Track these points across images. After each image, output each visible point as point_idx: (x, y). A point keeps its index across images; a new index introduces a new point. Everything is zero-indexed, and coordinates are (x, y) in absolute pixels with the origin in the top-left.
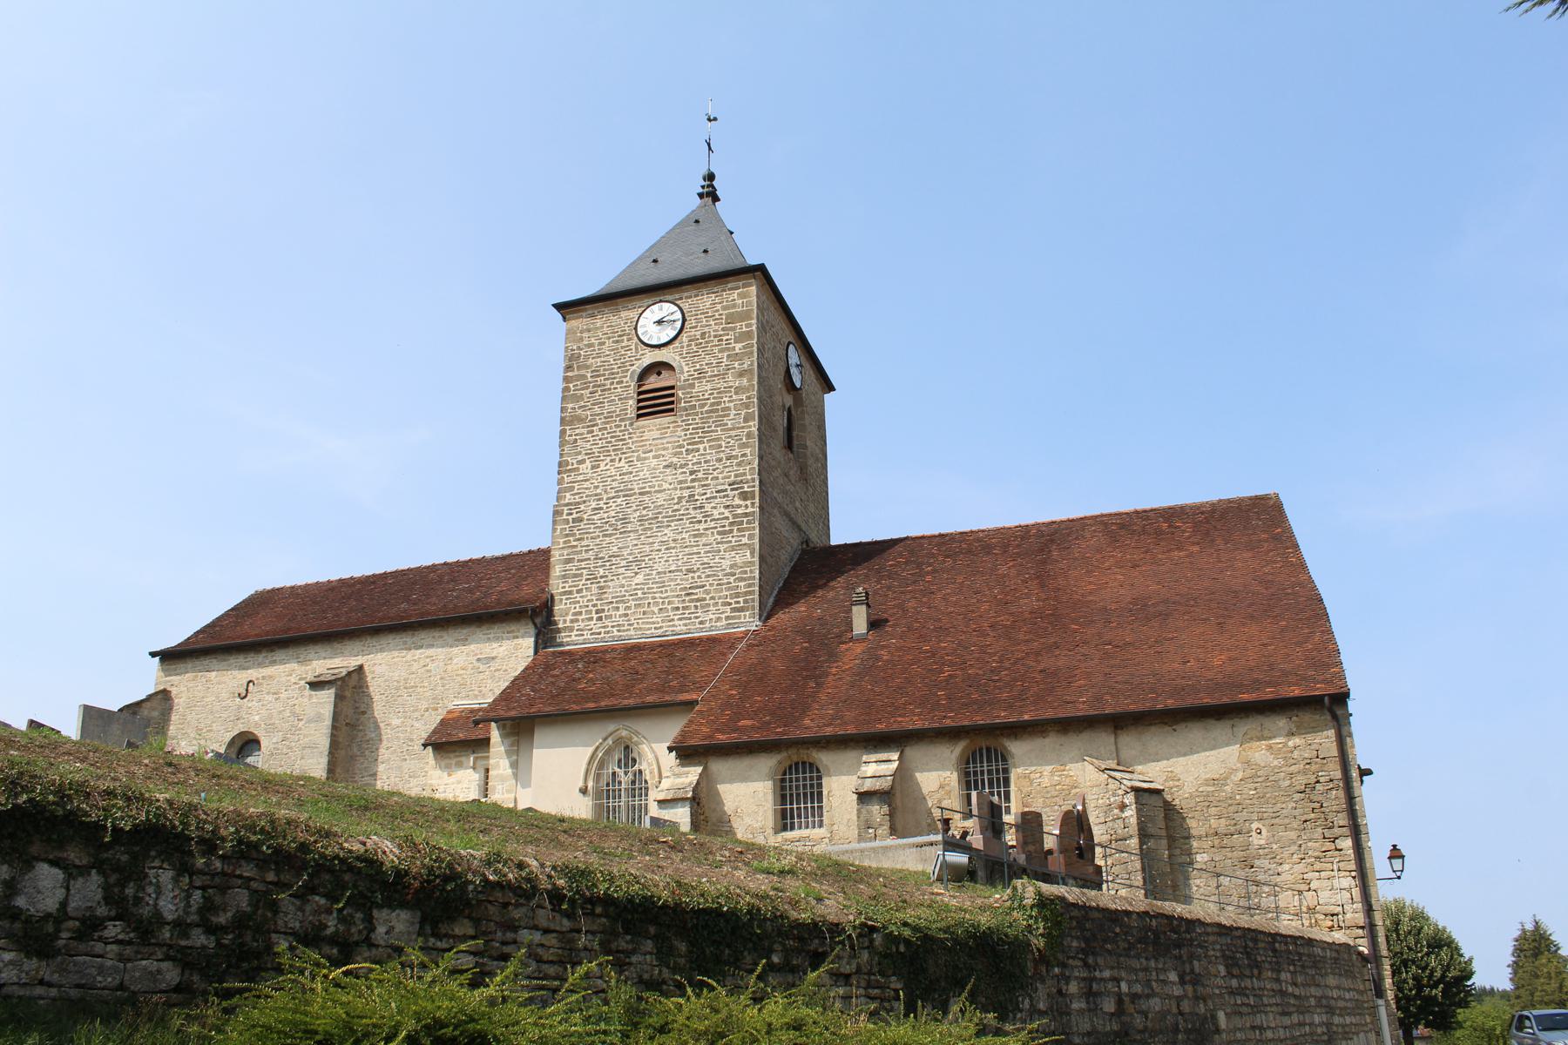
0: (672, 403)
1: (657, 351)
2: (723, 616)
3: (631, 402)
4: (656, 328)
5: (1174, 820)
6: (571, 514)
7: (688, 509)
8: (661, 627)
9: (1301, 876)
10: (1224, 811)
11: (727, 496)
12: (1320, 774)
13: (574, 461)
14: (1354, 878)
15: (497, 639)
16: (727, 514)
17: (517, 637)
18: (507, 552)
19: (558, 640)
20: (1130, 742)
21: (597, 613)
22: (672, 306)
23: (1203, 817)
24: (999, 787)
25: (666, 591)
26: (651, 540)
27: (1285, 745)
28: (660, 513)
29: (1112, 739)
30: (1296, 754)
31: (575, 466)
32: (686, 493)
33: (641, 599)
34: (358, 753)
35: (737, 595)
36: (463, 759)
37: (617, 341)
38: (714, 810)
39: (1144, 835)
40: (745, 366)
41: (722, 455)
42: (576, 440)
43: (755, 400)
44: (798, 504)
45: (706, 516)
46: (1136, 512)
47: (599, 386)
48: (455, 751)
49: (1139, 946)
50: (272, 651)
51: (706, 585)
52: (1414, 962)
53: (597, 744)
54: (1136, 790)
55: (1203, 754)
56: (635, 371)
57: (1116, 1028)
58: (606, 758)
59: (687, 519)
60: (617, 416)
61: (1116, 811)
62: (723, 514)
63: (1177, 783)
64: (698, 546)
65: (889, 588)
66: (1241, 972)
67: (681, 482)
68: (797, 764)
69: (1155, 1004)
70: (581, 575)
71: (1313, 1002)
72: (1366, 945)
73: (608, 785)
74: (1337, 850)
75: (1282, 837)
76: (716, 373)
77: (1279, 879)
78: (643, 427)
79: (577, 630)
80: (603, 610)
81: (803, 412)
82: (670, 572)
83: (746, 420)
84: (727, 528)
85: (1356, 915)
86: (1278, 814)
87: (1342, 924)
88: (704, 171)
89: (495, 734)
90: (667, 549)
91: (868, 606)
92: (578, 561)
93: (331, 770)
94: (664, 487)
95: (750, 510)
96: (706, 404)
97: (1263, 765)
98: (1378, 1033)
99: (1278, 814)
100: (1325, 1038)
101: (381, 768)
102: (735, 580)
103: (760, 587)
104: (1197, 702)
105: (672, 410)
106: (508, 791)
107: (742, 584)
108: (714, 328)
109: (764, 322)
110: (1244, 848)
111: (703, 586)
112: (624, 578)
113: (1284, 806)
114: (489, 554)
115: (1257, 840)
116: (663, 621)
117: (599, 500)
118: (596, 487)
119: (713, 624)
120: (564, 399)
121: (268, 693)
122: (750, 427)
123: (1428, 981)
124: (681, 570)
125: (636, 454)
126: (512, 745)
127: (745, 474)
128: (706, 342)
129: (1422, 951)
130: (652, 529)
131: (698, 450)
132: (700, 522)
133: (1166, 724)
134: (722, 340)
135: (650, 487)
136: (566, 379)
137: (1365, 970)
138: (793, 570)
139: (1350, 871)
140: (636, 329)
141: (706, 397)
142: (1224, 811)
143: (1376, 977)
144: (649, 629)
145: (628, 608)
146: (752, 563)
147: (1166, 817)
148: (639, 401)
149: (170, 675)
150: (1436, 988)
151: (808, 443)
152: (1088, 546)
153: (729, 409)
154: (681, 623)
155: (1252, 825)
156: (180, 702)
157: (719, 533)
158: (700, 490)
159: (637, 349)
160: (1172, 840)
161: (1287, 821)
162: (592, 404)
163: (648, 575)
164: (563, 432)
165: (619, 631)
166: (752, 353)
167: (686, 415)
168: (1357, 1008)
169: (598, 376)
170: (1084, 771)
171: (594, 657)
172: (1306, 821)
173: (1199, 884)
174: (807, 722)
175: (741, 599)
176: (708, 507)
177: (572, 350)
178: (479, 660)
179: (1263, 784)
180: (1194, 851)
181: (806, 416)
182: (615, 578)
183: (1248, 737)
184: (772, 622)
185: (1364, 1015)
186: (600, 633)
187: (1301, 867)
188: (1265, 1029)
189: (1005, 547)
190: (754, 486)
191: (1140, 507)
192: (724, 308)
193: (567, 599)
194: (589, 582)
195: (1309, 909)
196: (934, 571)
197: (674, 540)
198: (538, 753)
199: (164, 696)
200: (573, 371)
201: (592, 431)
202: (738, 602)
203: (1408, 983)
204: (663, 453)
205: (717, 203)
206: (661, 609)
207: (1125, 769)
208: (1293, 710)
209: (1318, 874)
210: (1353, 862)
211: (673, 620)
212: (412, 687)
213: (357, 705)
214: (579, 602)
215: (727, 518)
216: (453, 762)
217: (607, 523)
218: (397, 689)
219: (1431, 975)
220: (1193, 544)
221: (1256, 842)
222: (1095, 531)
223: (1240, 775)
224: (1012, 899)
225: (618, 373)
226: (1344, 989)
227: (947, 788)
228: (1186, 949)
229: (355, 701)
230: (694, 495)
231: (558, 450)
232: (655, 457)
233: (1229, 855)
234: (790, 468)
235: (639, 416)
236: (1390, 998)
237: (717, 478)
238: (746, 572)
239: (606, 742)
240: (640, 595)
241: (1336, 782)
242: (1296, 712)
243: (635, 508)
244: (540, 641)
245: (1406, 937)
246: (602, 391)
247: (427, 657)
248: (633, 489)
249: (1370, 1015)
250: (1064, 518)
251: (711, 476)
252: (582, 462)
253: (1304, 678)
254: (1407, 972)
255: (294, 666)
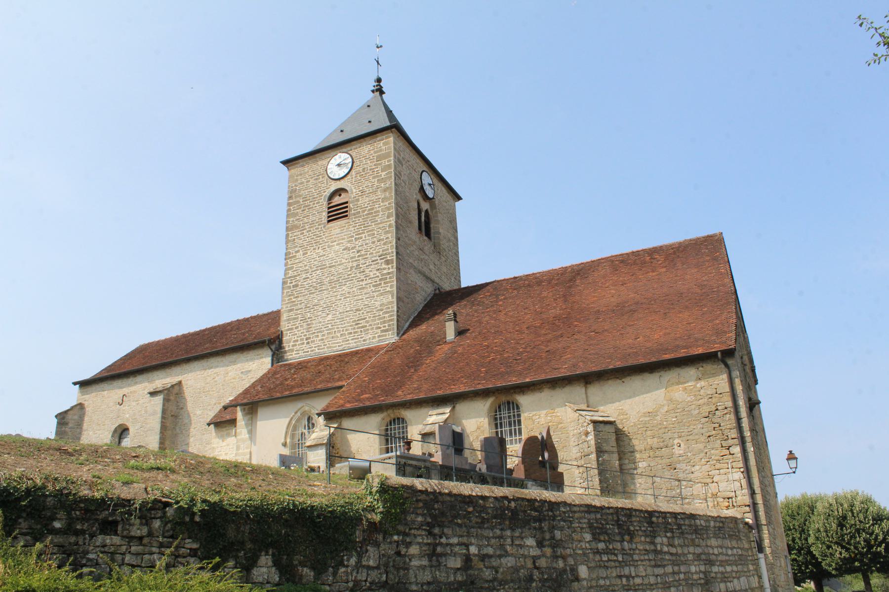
0: (347, 212)
1: (338, 182)
2: (376, 335)
3: (324, 214)
4: (336, 168)
5: (624, 441)
6: (292, 283)
7: (356, 273)
8: (342, 345)
9: (707, 473)
10: (656, 433)
11: (378, 263)
12: (718, 404)
13: (294, 252)
14: (742, 472)
15: (252, 360)
16: (378, 274)
17: (262, 358)
18: (270, 311)
19: (285, 358)
20: (596, 391)
21: (306, 340)
22: (346, 154)
23: (642, 438)
24: (515, 426)
25: (345, 323)
26: (336, 294)
27: (695, 386)
28: (341, 277)
29: (583, 390)
30: (702, 392)
31: (294, 254)
32: (355, 264)
33: (330, 329)
34: (179, 432)
35: (384, 322)
36: (230, 431)
37: (317, 179)
38: (346, 451)
39: (600, 451)
40: (387, 185)
41: (375, 239)
42: (294, 240)
43: (393, 205)
44: (432, 267)
45: (366, 277)
46: (633, 252)
47: (307, 206)
48: (226, 427)
49: (494, 520)
50: (135, 377)
51: (366, 318)
52: (864, 530)
53: (292, 416)
54: (595, 422)
55: (642, 396)
56: (326, 195)
57: (460, 579)
58: (297, 424)
59: (356, 279)
60: (317, 223)
61: (584, 437)
62: (376, 274)
63: (626, 417)
64: (362, 295)
65: (476, 311)
66: (610, 538)
67: (352, 258)
68: (394, 420)
69: (509, 562)
70: (297, 318)
71: (690, 557)
72: (751, 517)
73: (299, 441)
74: (730, 454)
75: (694, 448)
76: (371, 191)
77: (692, 476)
78: (331, 227)
79: (296, 351)
80: (310, 338)
81: (436, 213)
82: (346, 312)
83: (388, 217)
84: (378, 283)
85: (744, 497)
86: (691, 433)
87: (735, 504)
88: (376, 78)
89: (239, 415)
90: (345, 298)
91: (456, 321)
92: (296, 310)
93: (162, 442)
94: (343, 262)
95: (391, 270)
96: (366, 210)
97: (680, 400)
98: (760, 577)
99: (691, 433)
100: (702, 581)
101: (191, 440)
102: (383, 313)
103: (398, 316)
104: (635, 362)
105: (347, 216)
106: (247, 448)
107: (387, 315)
108: (369, 164)
109: (401, 158)
110: (670, 457)
111: (365, 319)
112: (321, 318)
113: (695, 427)
114: (261, 313)
115: (677, 451)
116: (343, 342)
117: (307, 273)
118: (306, 266)
119: (371, 341)
120: (288, 216)
121: (133, 401)
122: (390, 221)
123: (875, 542)
124: (352, 310)
125: (327, 244)
126: (248, 420)
127: (388, 249)
128: (366, 174)
129: (869, 523)
130: (336, 287)
131: (361, 238)
132: (363, 280)
133: (618, 378)
134: (374, 171)
135: (335, 262)
136: (289, 204)
137: (751, 535)
138: (426, 306)
139: (740, 468)
140: (326, 171)
141: (366, 206)
142: (656, 433)
143: (758, 540)
144: (336, 347)
145: (323, 335)
146: (392, 302)
147: (618, 440)
148: (329, 212)
149: (84, 395)
150: (880, 547)
151: (441, 231)
152: (598, 275)
153: (378, 211)
154: (353, 341)
155: (675, 441)
156: (89, 410)
157: (374, 286)
158: (363, 261)
159: (327, 182)
160: (621, 455)
161: (697, 437)
162: (303, 217)
163: (334, 315)
164: (287, 236)
165: (318, 349)
166: (391, 177)
167: (355, 218)
168: (741, 560)
169: (306, 200)
170: (566, 413)
171: (302, 366)
172: (709, 436)
173: (641, 484)
174: (400, 393)
175: (386, 325)
176: (367, 271)
177: (292, 187)
178: (242, 372)
179: (681, 414)
180: (637, 461)
181: (439, 215)
182: (316, 318)
183: (671, 383)
184: (405, 336)
185: (747, 565)
186: (308, 352)
187: (706, 468)
188: (633, 578)
189: (549, 281)
190: (393, 256)
191: (635, 249)
192: (375, 152)
193: (290, 333)
194: (302, 322)
195: (713, 495)
196: (504, 299)
197: (348, 293)
198: (259, 423)
199: (80, 406)
200: (292, 199)
201: (303, 233)
202: (385, 326)
203: (861, 544)
204: (342, 241)
205: (383, 95)
206: (342, 334)
207: (592, 409)
208: (699, 363)
209: (718, 471)
210: (741, 462)
211: (348, 340)
212: (207, 392)
213: (179, 404)
214: (296, 334)
215: (378, 276)
216: (225, 433)
217: (311, 286)
218: (200, 393)
219: (876, 539)
220: (663, 267)
221: (677, 452)
222: (605, 266)
223: (666, 408)
224: (366, 488)
225: (317, 198)
226: (727, 548)
227: (482, 429)
228: (547, 523)
229: (178, 402)
230: (359, 265)
231: (285, 246)
232: (338, 244)
233: (660, 462)
234: (425, 245)
235: (329, 221)
236: (768, 553)
237: (372, 253)
238: (389, 308)
239: (297, 414)
240: (330, 327)
241: (729, 409)
242: (701, 364)
243: (327, 276)
244: (275, 359)
245: (858, 514)
246: (308, 209)
247: (215, 373)
248: (325, 265)
249: (752, 564)
250: (589, 260)
251: (369, 253)
252: (297, 252)
253: (708, 342)
254: (860, 537)
255: (146, 384)
